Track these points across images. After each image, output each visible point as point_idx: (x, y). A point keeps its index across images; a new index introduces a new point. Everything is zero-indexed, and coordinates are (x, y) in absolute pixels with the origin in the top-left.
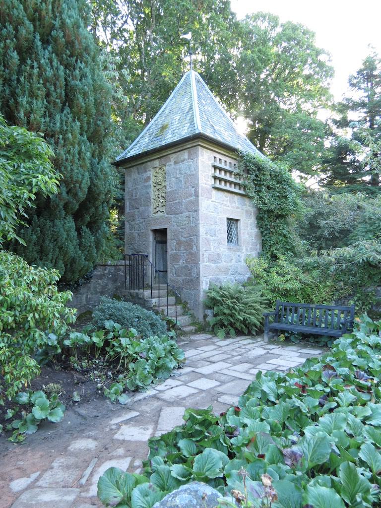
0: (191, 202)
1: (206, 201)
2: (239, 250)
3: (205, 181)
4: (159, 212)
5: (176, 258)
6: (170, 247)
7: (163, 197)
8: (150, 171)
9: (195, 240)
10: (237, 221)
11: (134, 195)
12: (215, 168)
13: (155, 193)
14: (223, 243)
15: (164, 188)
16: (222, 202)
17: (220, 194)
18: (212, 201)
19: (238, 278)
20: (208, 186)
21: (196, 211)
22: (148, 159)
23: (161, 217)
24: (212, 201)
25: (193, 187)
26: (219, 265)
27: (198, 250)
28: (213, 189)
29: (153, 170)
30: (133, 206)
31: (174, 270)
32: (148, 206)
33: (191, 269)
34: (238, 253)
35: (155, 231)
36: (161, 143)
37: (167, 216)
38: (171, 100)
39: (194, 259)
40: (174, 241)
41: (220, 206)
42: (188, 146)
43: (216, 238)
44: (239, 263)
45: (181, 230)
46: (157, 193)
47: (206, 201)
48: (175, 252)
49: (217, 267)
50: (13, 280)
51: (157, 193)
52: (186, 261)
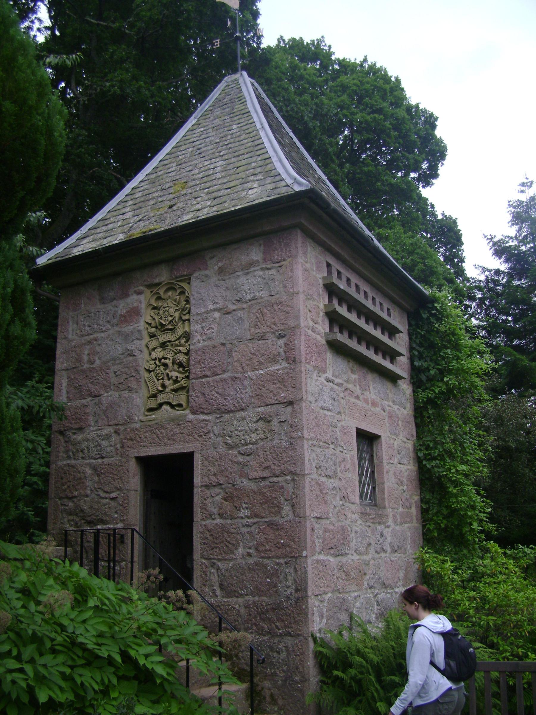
0: (278, 379)
1: (315, 377)
3: (311, 323)
4: (166, 407)
5: (222, 542)
6: (204, 507)
7: (180, 365)
8: (139, 293)
9: (289, 488)
11: (85, 358)
13: (154, 355)
14: (351, 497)
15: (183, 341)
18: (328, 381)
20: (318, 337)
21: (291, 403)
23: (173, 420)
24: (328, 381)
25: (281, 337)
26: (344, 559)
27: (301, 517)
29: (148, 292)
30: (79, 389)
31: (215, 578)
32: (130, 389)
33: (275, 573)
35: (146, 463)
36: (199, 214)
37: (191, 417)
39: (285, 545)
40: (217, 490)
41: (342, 395)
42: (267, 228)
44: (383, 555)
45: (240, 459)
46: (159, 353)
47: (315, 377)
48: (218, 521)
49: (341, 567)
50: (79, 682)
51: (159, 353)
52: (257, 550)
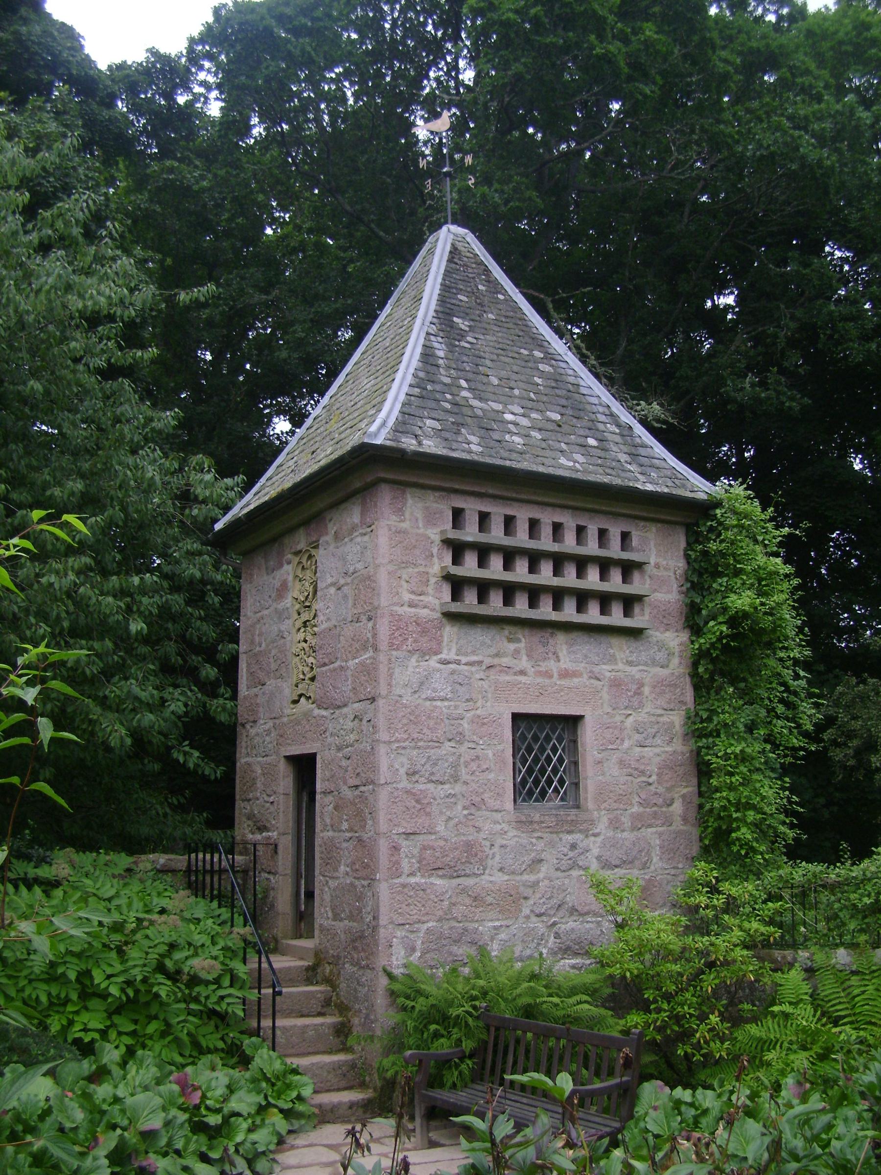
2: (572, 827)
10: (574, 721)
12: (458, 549)
16: (488, 661)
17: (479, 636)
19: (571, 924)
22: (413, 479)
28: (444, 620)
34: (570, 838)
38: (382, 325)
43: (458, 788)
